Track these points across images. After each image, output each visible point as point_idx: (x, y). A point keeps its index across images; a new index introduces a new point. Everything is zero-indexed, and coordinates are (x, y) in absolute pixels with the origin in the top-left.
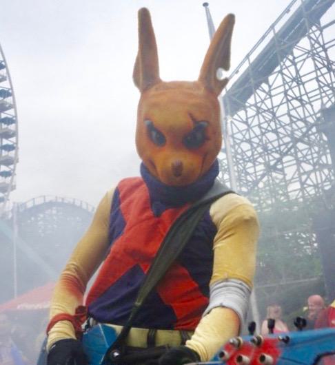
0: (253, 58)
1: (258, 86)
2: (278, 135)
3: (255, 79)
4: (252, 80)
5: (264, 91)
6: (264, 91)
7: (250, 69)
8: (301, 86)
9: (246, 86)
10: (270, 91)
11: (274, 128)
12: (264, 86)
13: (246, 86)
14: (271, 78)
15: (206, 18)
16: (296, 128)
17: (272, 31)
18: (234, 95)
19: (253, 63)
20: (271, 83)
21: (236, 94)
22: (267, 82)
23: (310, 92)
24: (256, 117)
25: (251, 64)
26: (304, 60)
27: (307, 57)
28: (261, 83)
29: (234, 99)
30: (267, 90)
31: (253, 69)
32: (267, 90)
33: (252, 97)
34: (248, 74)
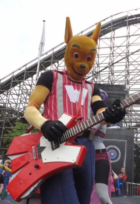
0: (55, 50)
1: (54, 63)
2: (31, 88)
3: (53, 60)
4: (52, 59)
5: (55, 66)
6: (55, 66)
7: (53, 55)
8: (98, 68)
9: (49, 61)
10: (58, 67)
11: (31, 84)
12: (56, 64)
13: (49, 61)
14: (60, 62)
15: (43, 27)
16: (25, 88)
17: (52, 51)
18: (42, 63)
19: (54, 52)
20: (59, 64)
21: (43, 63)
22: (58, 63)
23: (115, 71)
24: (100, 63)
25: (26, 69)
26: (132, 43)
27: (131, 44)
28: (55, 62)
29: (42, 65)
30: (57, 66)
31: (54, 55)
32: (57, 66)
33: (50, 66)
34: (51, 56)
